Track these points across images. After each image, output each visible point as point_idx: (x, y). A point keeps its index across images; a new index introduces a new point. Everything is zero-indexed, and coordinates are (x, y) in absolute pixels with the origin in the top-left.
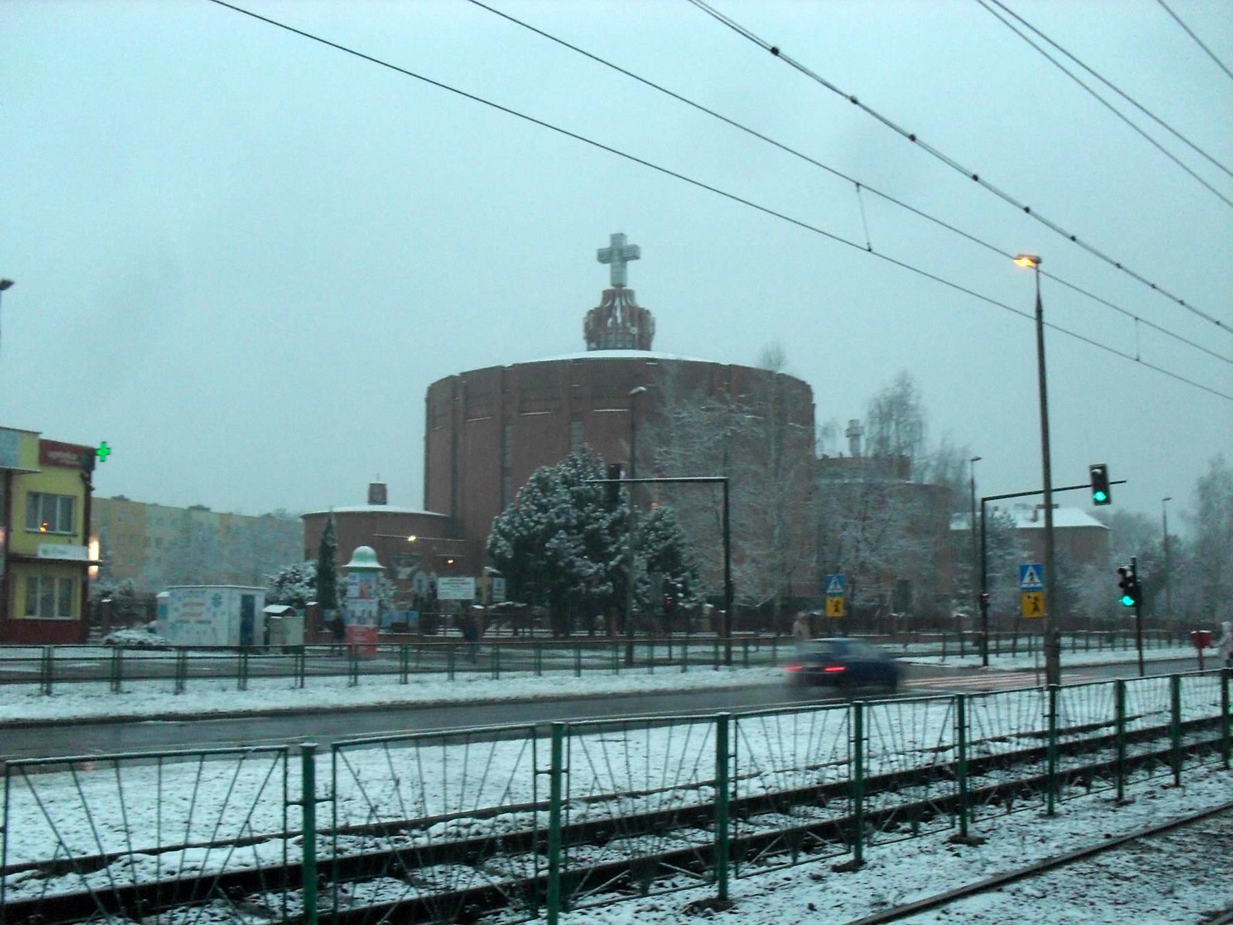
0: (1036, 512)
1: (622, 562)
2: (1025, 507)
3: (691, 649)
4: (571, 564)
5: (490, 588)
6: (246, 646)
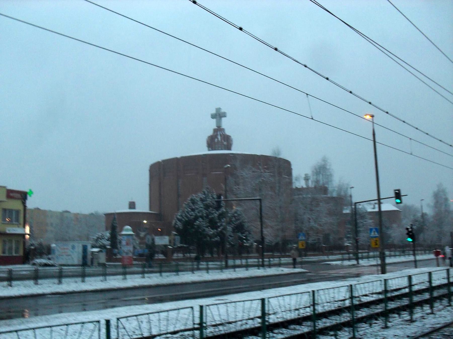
0: (374, 206)
1: (223, 229)
2: (371, 204)
3: (249, 260)
4: (204, 230)
5: (174, 240)
6: (84, 264)
